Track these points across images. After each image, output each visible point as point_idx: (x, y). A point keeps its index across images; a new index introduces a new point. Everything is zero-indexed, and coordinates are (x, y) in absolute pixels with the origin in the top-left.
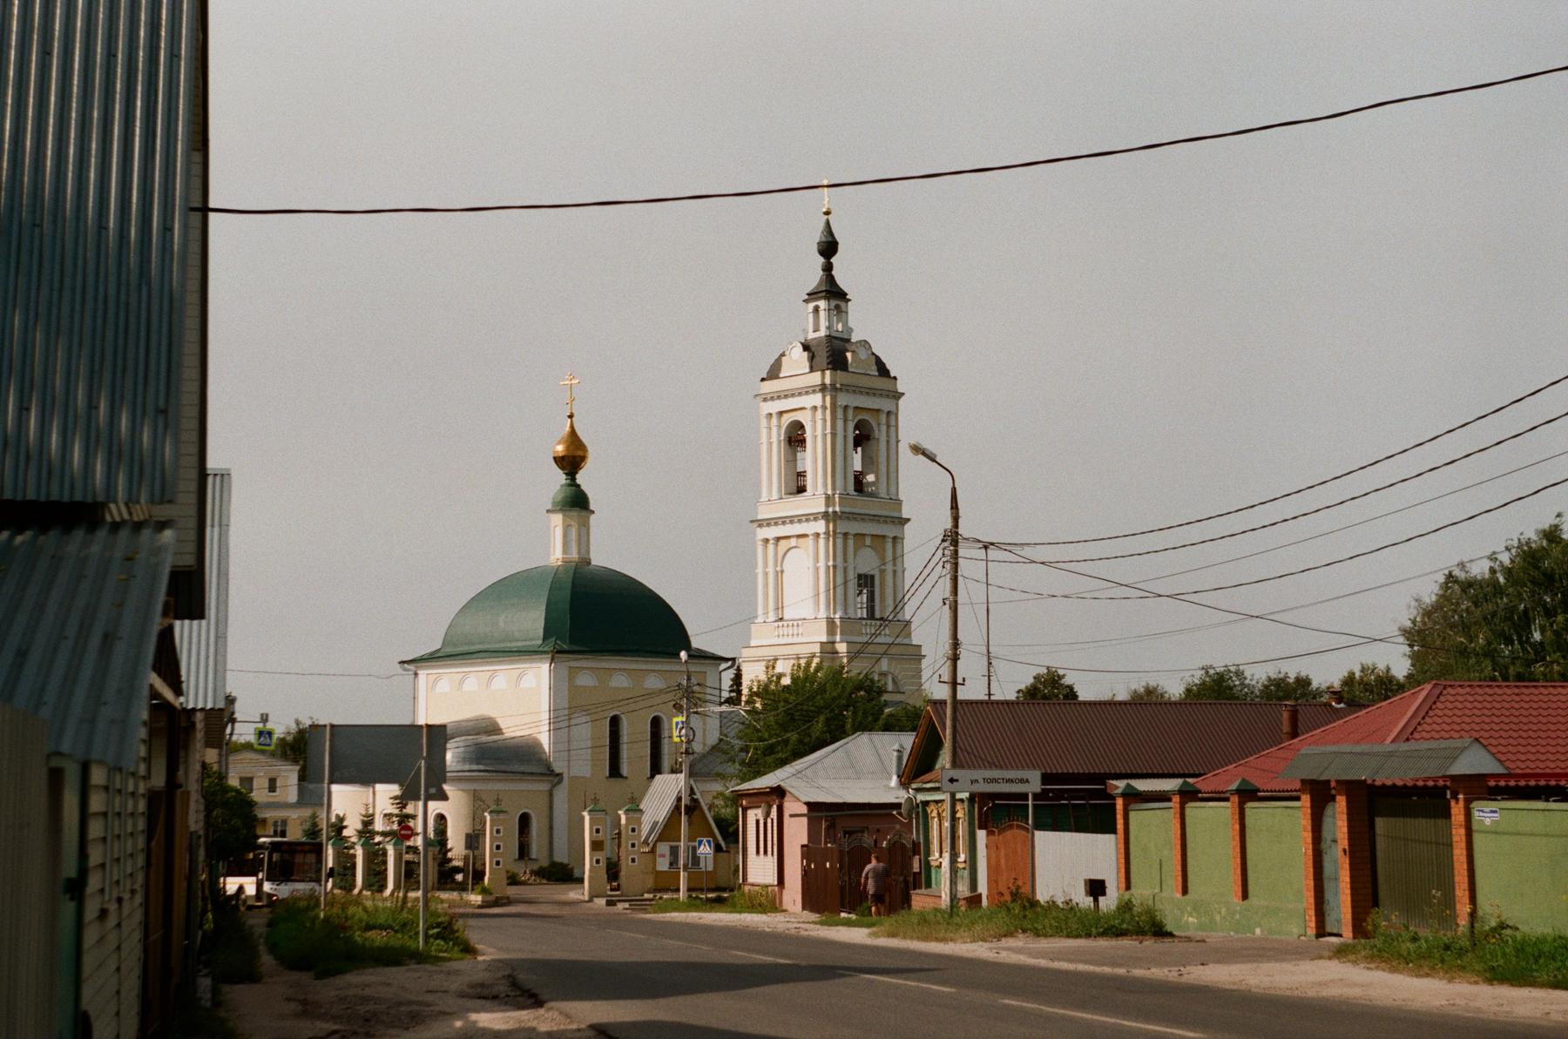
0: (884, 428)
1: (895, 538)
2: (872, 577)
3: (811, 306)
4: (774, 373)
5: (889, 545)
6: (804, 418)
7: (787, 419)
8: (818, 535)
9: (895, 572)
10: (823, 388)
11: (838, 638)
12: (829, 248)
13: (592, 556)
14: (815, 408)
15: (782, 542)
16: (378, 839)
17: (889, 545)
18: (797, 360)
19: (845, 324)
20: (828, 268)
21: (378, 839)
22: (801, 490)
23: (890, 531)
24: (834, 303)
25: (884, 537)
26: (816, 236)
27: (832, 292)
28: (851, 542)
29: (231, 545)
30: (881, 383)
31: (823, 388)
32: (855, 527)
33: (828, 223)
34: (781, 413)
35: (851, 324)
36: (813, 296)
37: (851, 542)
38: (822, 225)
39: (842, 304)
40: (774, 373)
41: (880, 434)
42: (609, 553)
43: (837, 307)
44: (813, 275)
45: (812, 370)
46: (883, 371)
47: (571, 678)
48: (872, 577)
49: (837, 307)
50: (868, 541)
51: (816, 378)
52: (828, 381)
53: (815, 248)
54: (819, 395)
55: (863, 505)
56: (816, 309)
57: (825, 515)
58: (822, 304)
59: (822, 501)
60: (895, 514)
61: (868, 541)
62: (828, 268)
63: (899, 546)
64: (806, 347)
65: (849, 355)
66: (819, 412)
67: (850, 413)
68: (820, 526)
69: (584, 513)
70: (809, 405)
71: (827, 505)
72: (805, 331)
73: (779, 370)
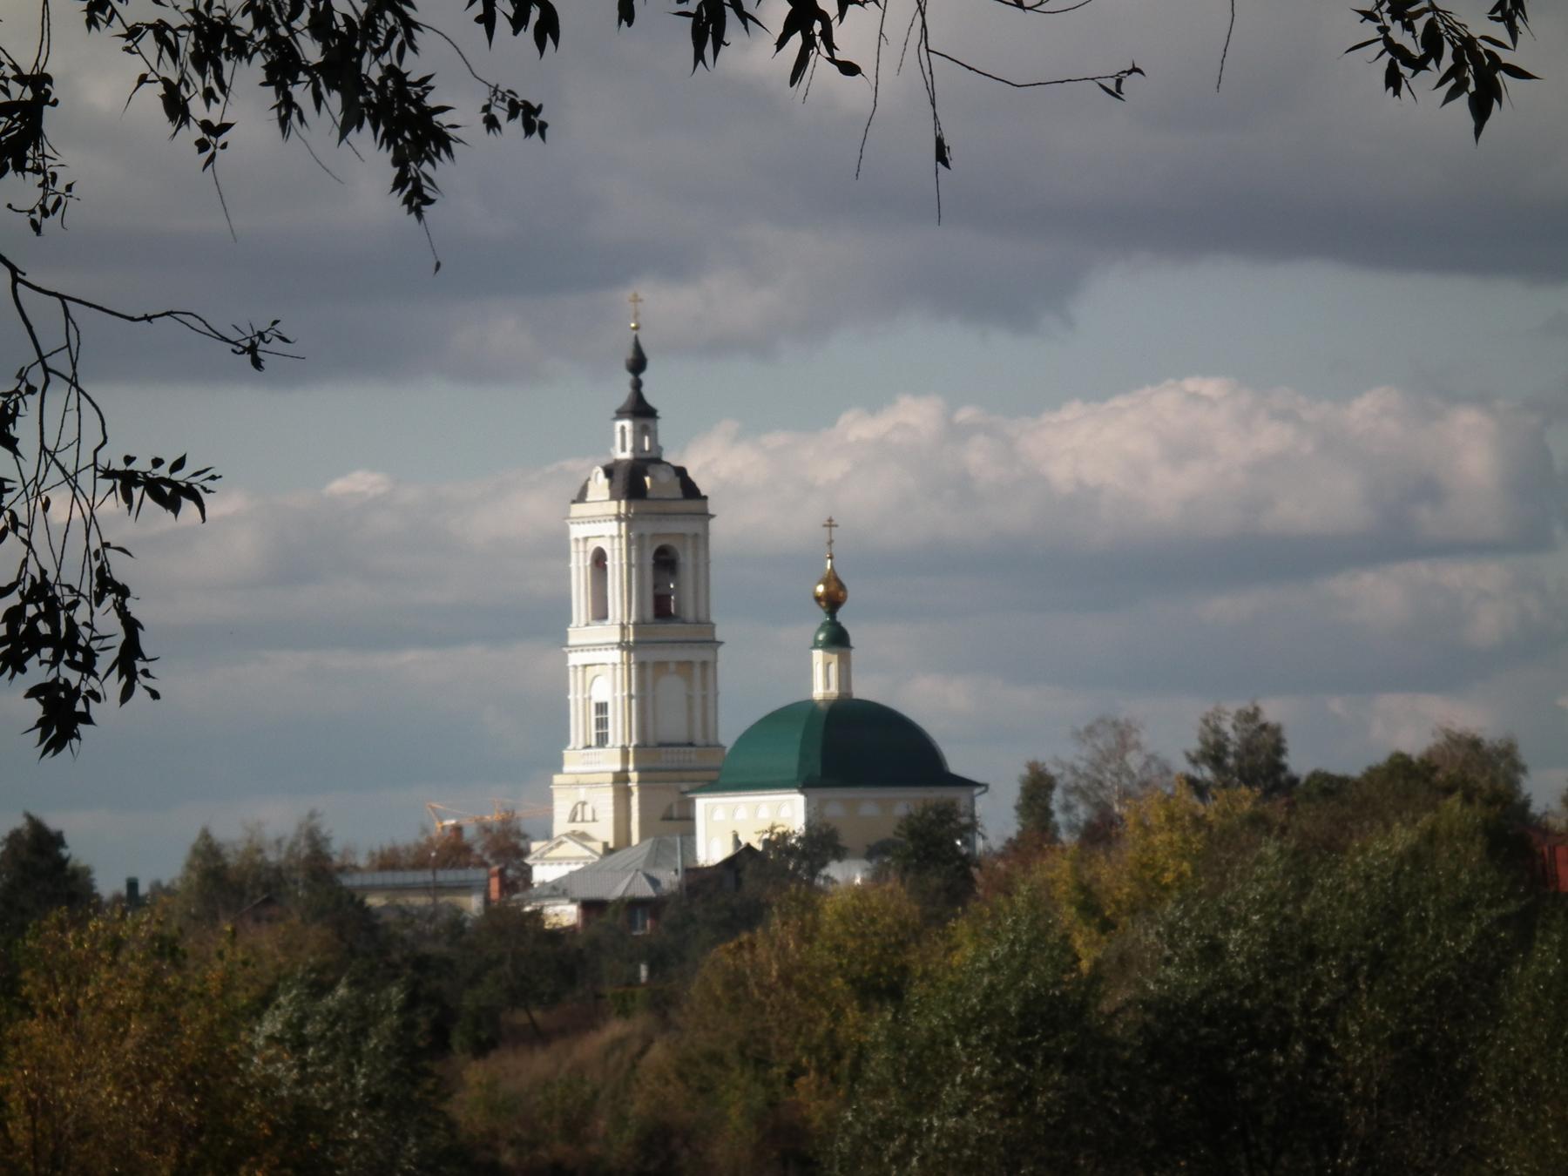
5: (697, 671)
7: (593, 545)
9: (704, 697)
10: (618, 518)
11: (631, 766)
14: (612, 537)
16: (124, 1103)
17: (697, 671)
19: (654, 441)
20: (637, 385)
21: (124, 1103)
22: (605, 617)
23: (696, 655)
26: (628, 353)
27: (640, 411)
28: (649, 672)
30: (692, 505)
34: (586, 539)
35: (662, 441)
37: (649, 672)
38: (632, 340)
40: (582, 497)
41: (686, 559)
44: (621, 392)
46: (690, 490)
47: (149, 26)
52: (623, 510)
54: (615, 524)
55: (669, 630)
58: (627, 424)
59: (617, 629)
62: (637, 385)
63: (710, 672)
64: (609, 472)
65: (647, 479)
69: (844, 650)
70: (607, 534)
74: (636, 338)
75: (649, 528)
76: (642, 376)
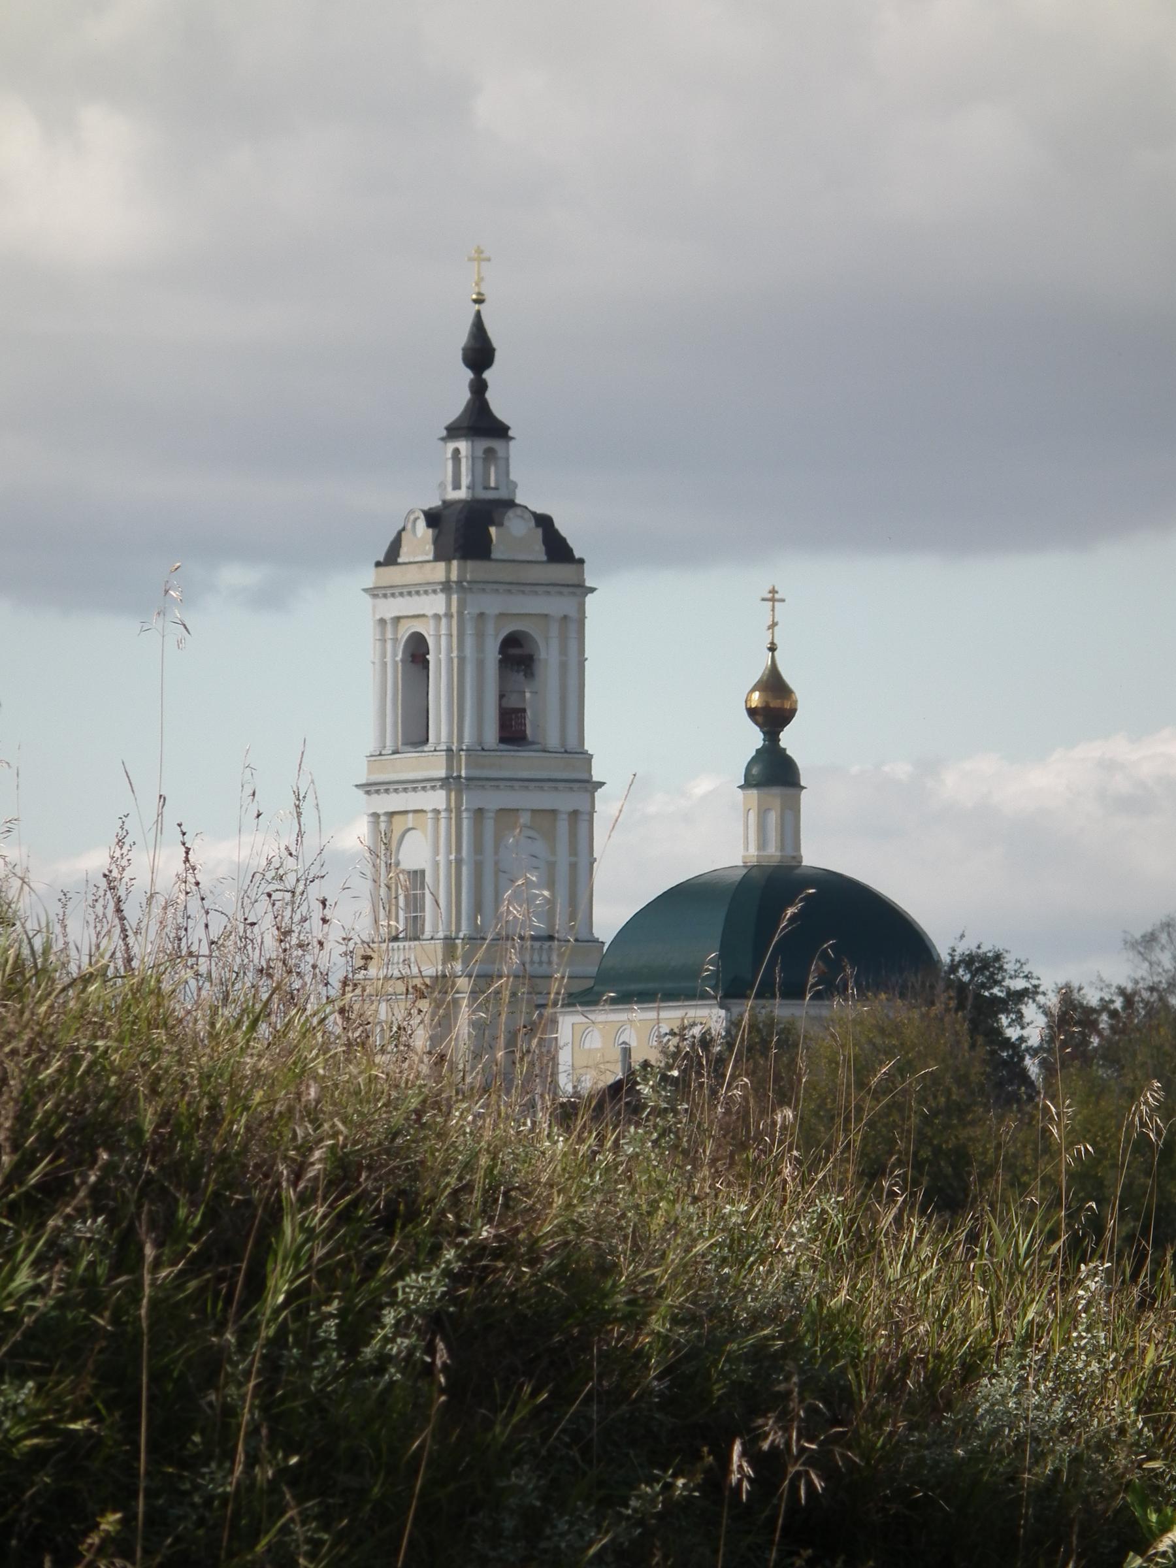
0: (554, 644)
1: (575, 814)
2: (423, 872)
3: (451, 446)
4: (392, 557)
6: (427, 630)
7: (406, 630)
8: (437, 812)
10: (446, 587)
12: (479, 354)
13: (804, 851)
15: (396, 819)
17: (563, 826)
18: (421, 538)
20: (479, 388)
23: (564, 802)
24: (483, 444)
25: (554, 812)
27: (480, 424)
28: (489, 825)
29: (906, 909)
30: (560, 572)
31: (446, 587)
32: (494, 800)
33: (478, 315)
34: (397, 620)
36: (453, 432)
37: (489, 825)
38: (469, 320)
39: (496, 444)
40: (392, 557)
41: (548, 655)
42: (820, 852)
43: (490, 453)
44: (455, 399)
45: (437, 558)
48: (423, 872)
49: (490, 453)
50: (525, 819)
51: (438, 572)
52: (454, 577)
53: (459, 355)
54: (442, 597)
55: (520, 763)
56: (457, 451)
57: (446, 782)
58: (463, 446)
60: (584, 776)
61: (525, 819)
62: (479, 388)
66: (444, 621)
67: (490, 628)
68: (437, 799)
71: (449, 767)
72: (442, 485)
73: (398, 555)
74: (478, 315)
75: (493, 604)
76: (487, 375)
